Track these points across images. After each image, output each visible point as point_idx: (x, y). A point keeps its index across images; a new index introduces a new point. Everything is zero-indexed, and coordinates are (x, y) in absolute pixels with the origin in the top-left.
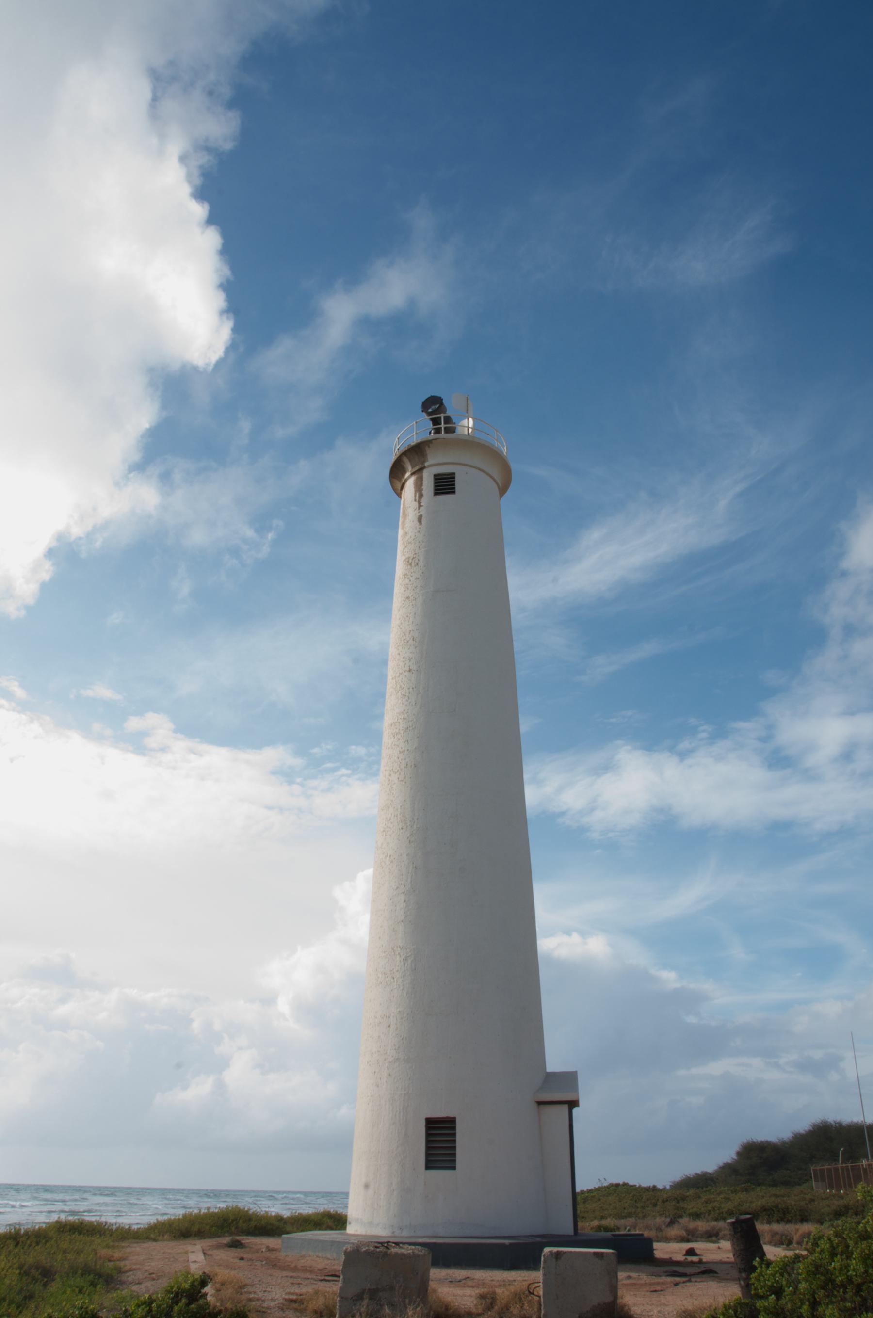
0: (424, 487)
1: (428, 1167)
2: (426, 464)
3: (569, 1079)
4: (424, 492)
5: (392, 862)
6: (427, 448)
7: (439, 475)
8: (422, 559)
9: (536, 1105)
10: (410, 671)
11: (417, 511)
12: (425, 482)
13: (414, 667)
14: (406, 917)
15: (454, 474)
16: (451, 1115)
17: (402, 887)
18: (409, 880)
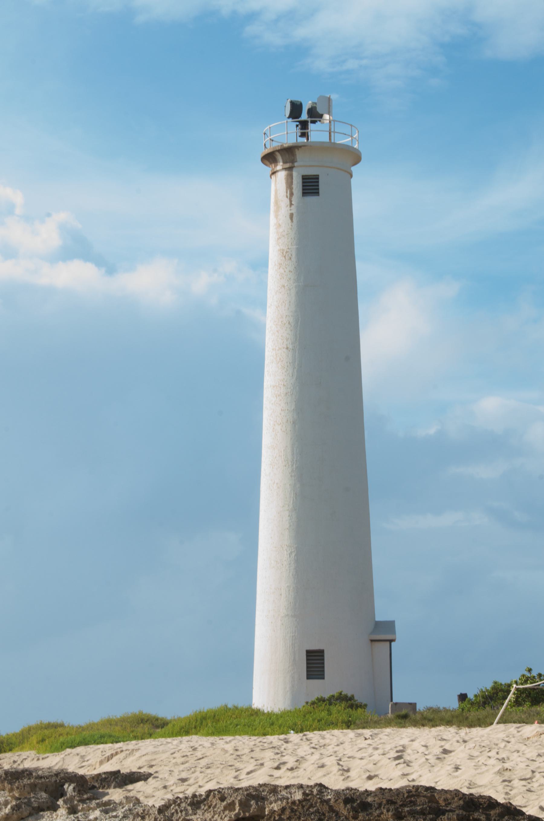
0: (294, 186)
1: (308, 678)
2: (296, 164)
3: (389, 626)
4: (295, 191)
5: (278, 488)
6: (296, 150)
7: (306, 176)
8: (294, 256)
9: (370, 642)
10: (287, 348)
11: (288, 208)
12: (295, 182)
13: (290, 347)
14: (290, 526)
15: (318, 175)
16: (321, 648)
17: (287, 506)
18: (292, 502)
